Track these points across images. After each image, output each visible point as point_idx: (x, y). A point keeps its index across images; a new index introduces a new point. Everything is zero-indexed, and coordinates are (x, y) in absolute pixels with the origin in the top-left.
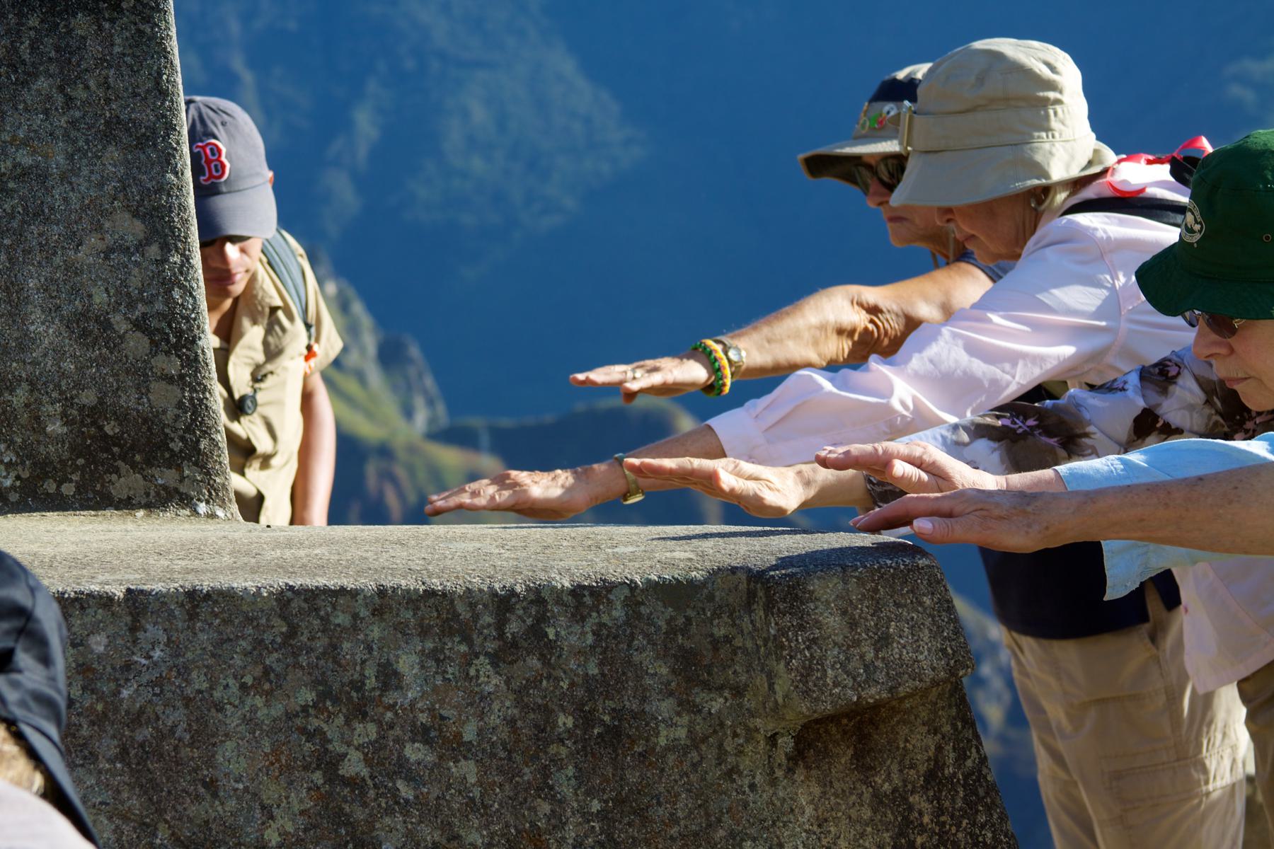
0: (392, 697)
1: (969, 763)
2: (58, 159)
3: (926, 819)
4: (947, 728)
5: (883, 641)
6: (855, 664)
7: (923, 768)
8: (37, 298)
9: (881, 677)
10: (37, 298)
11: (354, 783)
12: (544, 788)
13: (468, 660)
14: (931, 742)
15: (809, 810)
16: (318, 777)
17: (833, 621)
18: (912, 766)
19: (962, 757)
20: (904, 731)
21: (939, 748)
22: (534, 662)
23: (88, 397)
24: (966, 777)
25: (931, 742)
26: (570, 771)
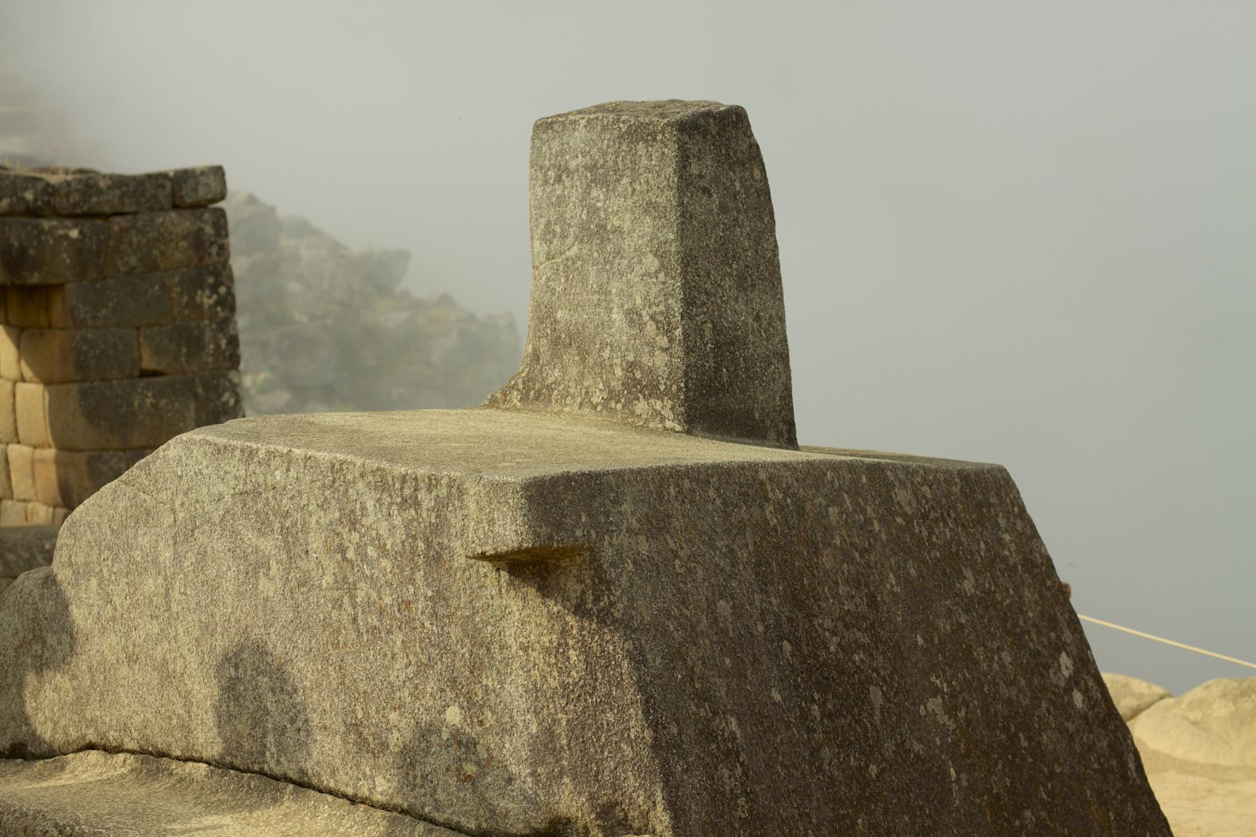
0: (364, 521)
1: (602, 604)
2: (627, 225)
3: (575, 632)
4: (588, 581)
5: (491, 522)
6: (481, 531)
7: (574, 602)
8: (616, 299)
9: (490, 541)
10: (616, 299)
11: (350, 561)
12: (412, 581)
13: (391, 504)
14: (579, 588)
15: (517, 614)
16: (339, 556)
17: (472, 506)
18: (568, 600)
19: (597, 599)
20: (563, 578)
21: (583, 592)
22: (413, 512)
23: (631, 358)
24: (599, 611)
25: (579, 588)
26: (422, 573)
